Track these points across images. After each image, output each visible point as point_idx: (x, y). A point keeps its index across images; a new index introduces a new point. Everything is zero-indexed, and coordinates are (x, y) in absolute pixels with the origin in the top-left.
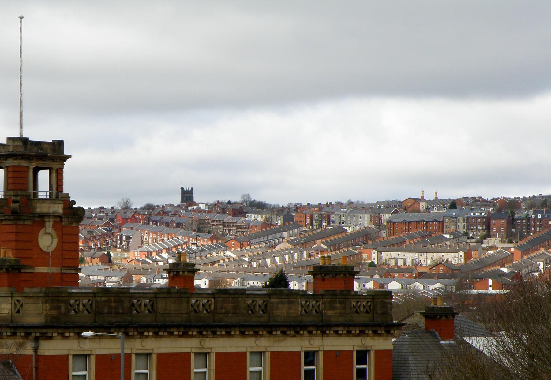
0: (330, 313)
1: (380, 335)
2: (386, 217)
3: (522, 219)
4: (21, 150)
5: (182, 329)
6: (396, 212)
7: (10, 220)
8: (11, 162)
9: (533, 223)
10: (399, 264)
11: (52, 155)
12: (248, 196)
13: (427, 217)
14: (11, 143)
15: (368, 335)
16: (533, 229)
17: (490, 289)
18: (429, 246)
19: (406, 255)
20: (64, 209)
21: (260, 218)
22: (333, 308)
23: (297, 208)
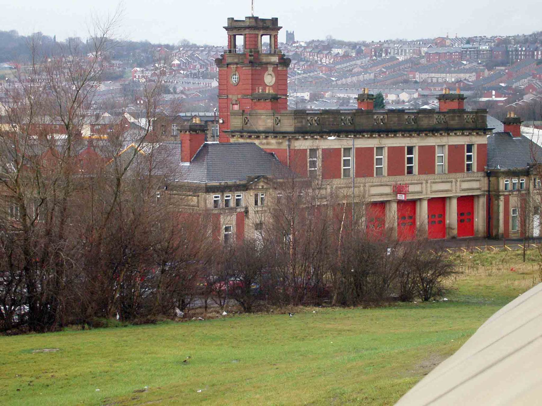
0: (452, 122)
1: (480, 135)
2: (424, 50)
3: (512, 51)
4: (253, 24)
5: (369, 133)
6: (431, 46)
7: (247, 66)
8: (247, 32)
9: (520, 53)
10: (433, 81)
11: (271, 26)
12: (331, 37)
13: (452, 50)
14: (248, 20)
15: (473, 135)
16: (520, 57)
17: (494, 97)
18: (453, 69)
19: (437, 75)
20: (279, 59)
21: (341, 51)
22: (453, 120)
23: (364, 44)
